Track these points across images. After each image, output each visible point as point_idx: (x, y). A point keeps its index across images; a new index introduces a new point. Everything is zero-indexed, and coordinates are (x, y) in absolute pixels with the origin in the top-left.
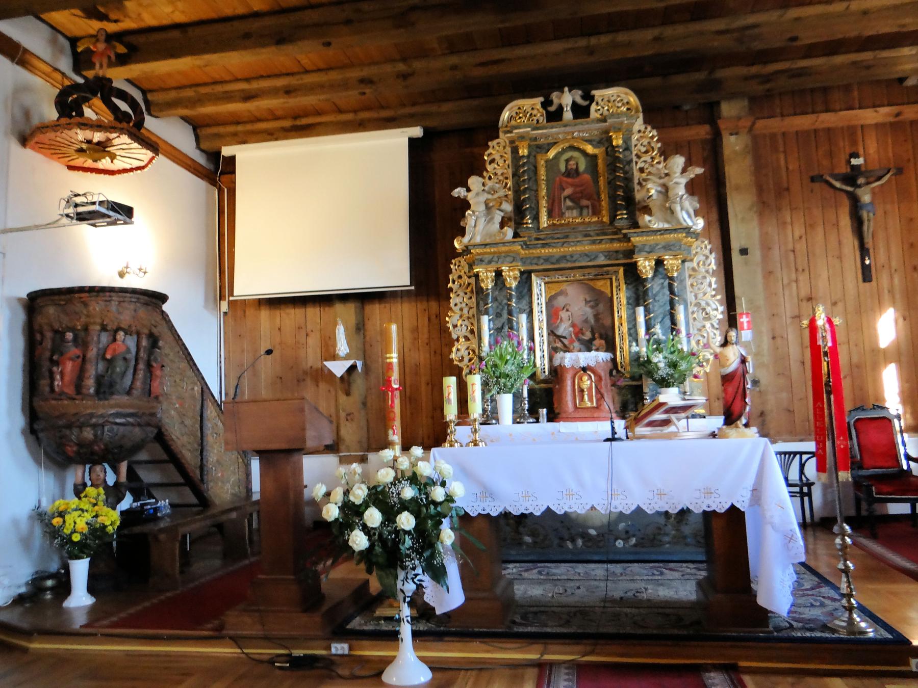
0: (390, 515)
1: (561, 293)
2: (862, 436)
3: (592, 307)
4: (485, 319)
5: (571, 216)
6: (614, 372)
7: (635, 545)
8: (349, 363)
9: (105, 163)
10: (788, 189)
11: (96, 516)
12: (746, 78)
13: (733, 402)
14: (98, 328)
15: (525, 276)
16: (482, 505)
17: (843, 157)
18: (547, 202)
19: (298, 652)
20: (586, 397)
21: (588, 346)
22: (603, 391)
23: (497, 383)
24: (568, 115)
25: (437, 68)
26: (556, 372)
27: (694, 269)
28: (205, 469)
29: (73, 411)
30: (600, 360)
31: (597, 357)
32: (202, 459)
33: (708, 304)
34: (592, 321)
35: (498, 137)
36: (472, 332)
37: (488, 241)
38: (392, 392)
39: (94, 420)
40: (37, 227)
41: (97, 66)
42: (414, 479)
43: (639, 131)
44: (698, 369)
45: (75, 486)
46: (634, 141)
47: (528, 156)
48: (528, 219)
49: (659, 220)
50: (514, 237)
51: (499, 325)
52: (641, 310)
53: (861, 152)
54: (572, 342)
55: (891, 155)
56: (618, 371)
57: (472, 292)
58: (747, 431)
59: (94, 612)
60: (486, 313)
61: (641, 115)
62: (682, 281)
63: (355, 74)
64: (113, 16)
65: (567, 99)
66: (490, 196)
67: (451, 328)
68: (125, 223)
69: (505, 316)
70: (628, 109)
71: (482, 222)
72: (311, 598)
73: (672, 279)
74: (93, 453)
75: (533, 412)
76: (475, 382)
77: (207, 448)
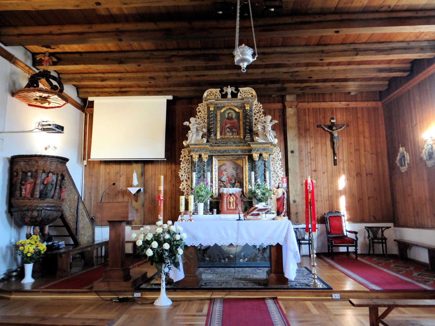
0: (161, 244)
1: (224, 164)
2: (331, 222)
3: (235, 170)
4: (194, 174)
5: (229, 135)
6: (242, 196)
7: (247, 261)
8: (138, 189)
9: (46, 105)
10: (309, 129)
11: (37, 246)
12: (296, 88)
13: (284, 208)
14: (41, 171)
15: (210, 157)
16: (192, 242)
17: (329, 119)
18: (220, 129)
19: (121, 297)
20: (231, 205)
21: (233, 186)
22: (238, 203)
23: (198, 199)
24: (229, 96)
25: (180, 76)
26: (221, 195)
27: (274, 158)
28: (78, 230)
29: (29, 204)
30: (237, 191)
31: (236, 190)
32: (77, 226)
33: (278, 171)
34: (235, 175)
35: (202, 102)
36: (189, 178)
37: (197, 143)
38: (161, 201)
39: (38, 208)
40: (24, 132)
41: (45, 65)
42: (169, 232)
43: (256, 104)
44: (273, 196)
45: (27, 235)
46: (253, 108)
47: (214, 111)
48: (212, 135)
49: (261, 139)
50: (207, 142)
51: (199, 176)
52: (253, 173)
53: (335, 118)
54: (227, 183)
55: (345, 119)
56: (244, 196)
57: (189, 162)
58: (284, 218)
59: (34, 286)
60: (195, 171)
61: (257, 98)
62: (269, 162)
63: (148, 75)
64: (52, 47)
65: (229, 90)
66: (198, 126)
67: (180, 176)
68: (61, 133)
69: (202, 172)
70: (252, 96)
71: (195, 135)
72: (127, 277)
73: (265, 161)
74: (36, 221)
75: (211, 210)
76: (191, 198)
77: (79, 221)
